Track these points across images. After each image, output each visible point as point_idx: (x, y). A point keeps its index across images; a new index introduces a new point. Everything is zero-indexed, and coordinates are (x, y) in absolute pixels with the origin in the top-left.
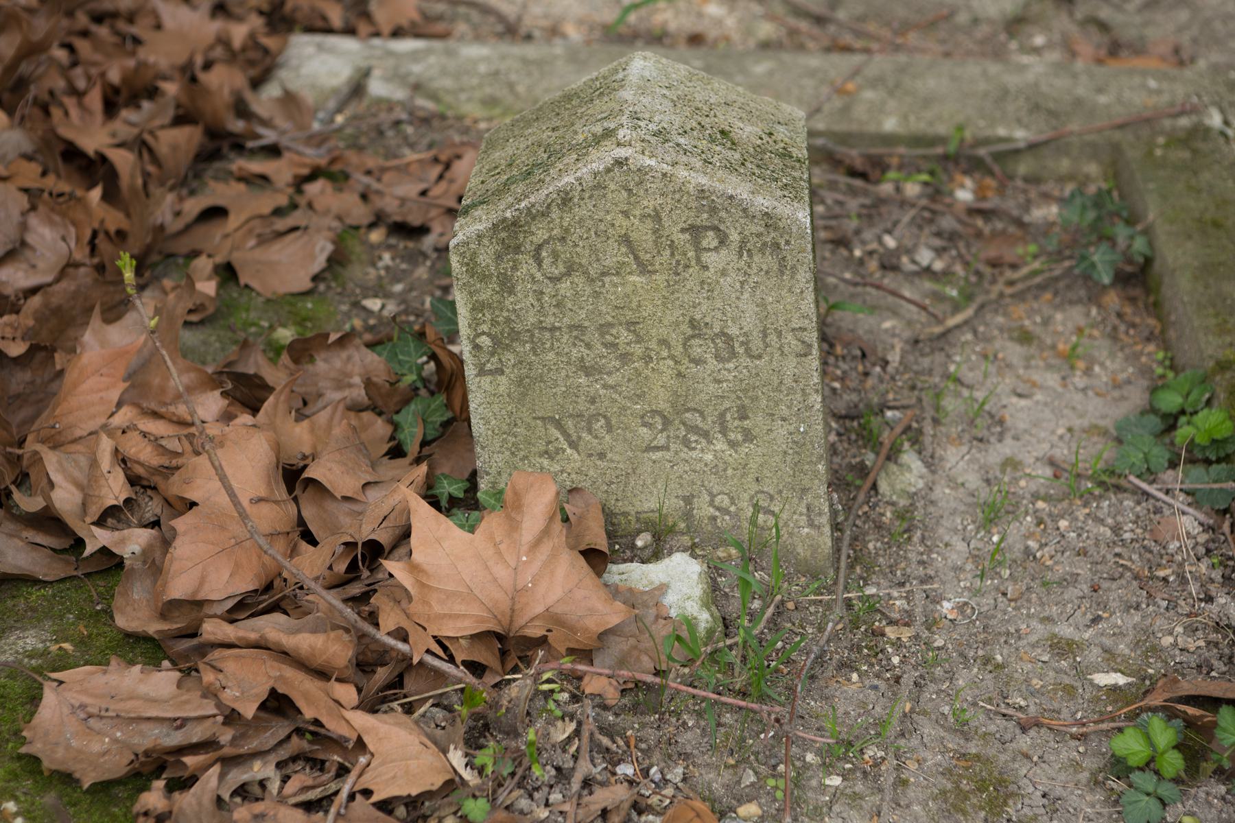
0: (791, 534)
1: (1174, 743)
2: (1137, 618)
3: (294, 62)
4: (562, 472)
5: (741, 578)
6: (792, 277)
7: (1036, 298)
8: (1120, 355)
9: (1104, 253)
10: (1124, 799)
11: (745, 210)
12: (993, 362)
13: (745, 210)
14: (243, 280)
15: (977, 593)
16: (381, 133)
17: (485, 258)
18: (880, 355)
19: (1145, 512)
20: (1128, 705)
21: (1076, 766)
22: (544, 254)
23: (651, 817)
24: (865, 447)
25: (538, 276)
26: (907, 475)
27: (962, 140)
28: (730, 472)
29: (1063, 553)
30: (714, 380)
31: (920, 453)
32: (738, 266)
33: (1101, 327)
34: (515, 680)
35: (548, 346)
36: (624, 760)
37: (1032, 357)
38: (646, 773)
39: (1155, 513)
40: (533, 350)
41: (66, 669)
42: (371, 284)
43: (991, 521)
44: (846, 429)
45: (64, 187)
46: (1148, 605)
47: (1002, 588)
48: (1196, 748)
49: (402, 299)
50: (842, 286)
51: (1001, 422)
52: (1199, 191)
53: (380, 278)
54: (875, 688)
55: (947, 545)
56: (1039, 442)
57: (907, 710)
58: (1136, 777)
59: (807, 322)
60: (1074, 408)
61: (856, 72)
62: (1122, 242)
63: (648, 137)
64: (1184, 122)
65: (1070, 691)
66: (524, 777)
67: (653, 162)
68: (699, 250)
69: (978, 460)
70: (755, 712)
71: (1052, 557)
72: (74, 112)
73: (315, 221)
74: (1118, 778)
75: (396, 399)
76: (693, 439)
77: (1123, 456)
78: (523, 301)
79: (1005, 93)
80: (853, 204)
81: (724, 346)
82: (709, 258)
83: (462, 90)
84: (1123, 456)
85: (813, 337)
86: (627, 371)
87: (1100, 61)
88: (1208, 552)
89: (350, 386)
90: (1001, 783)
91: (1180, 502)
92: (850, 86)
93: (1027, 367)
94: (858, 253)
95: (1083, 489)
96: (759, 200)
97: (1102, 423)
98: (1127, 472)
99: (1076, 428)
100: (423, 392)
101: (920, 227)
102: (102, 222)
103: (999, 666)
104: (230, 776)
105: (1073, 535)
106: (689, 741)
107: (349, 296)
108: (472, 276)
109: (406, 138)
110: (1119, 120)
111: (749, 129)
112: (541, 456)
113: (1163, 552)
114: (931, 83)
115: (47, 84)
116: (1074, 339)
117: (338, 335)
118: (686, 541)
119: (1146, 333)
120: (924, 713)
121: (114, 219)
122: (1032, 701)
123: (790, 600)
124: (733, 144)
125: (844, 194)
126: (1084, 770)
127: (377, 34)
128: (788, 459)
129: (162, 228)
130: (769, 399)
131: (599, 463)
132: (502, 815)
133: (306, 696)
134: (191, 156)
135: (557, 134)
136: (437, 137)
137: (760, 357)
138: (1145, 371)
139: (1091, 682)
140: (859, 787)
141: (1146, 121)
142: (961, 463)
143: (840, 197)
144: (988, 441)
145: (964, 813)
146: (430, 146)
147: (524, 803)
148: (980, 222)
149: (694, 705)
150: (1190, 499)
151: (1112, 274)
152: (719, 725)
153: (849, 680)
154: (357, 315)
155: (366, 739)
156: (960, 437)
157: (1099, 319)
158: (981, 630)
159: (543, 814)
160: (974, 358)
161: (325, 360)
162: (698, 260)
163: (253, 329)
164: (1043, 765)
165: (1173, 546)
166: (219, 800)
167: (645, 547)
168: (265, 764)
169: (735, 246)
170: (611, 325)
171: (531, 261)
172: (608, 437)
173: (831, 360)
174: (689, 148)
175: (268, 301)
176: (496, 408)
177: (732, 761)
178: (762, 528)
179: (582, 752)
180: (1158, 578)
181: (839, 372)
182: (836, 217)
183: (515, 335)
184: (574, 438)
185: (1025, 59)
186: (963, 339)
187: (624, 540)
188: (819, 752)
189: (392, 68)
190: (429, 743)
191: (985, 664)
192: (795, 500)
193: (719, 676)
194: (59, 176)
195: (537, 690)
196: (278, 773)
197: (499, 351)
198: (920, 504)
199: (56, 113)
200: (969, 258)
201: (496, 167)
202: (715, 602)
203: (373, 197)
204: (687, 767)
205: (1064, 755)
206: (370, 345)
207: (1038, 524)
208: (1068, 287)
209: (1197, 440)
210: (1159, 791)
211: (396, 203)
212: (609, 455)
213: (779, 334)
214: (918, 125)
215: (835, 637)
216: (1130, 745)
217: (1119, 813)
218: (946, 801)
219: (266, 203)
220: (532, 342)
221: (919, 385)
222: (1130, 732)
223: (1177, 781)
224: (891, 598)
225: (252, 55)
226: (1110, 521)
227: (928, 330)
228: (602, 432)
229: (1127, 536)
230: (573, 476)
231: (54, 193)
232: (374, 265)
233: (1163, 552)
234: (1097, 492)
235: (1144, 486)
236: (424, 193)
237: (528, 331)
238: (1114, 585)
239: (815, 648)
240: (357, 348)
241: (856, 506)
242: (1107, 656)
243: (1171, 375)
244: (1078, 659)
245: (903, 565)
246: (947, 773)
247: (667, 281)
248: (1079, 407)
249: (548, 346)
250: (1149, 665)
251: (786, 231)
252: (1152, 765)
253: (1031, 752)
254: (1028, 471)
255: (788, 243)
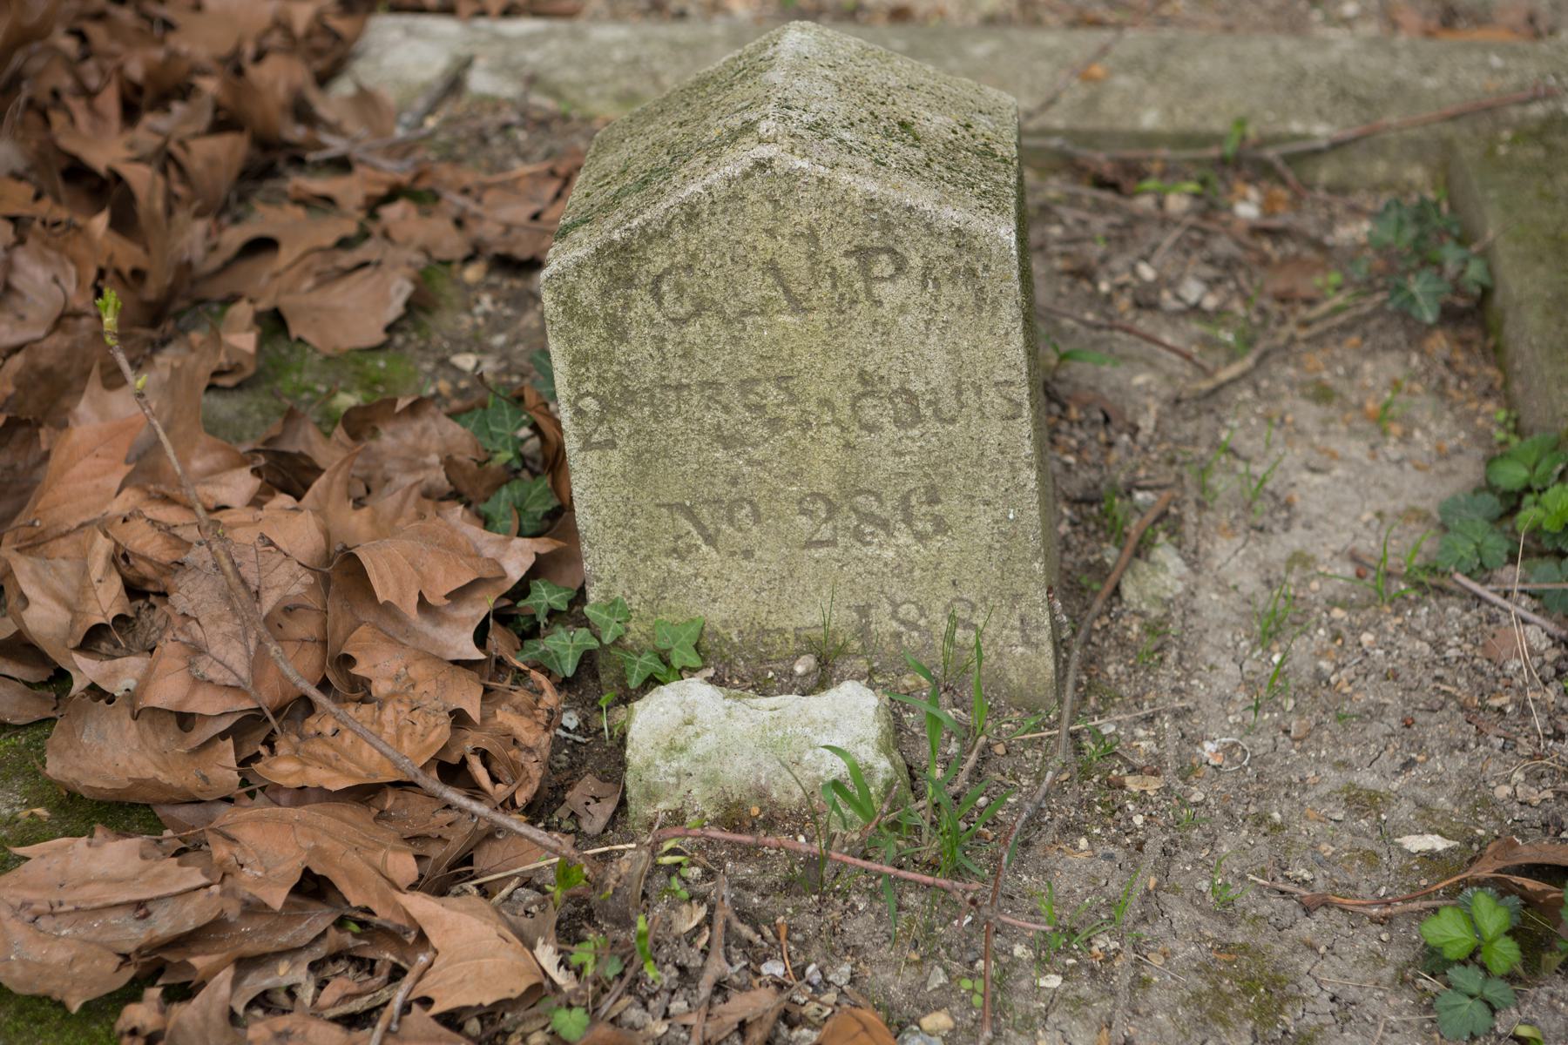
0: (1000, 655)
1: (1507, 928)
2: (1463, 762)
3: (374, 51)
4: (696, 576)
5: (928, 713)
6: (993, 315)
7: (1339, 342)
8: (1448, 415)
9: (1426, 283)
10: (1439, 1003)
11: (928, 226)
12: (1278, 427)
13: (928, 226)
14: (295, 331)
15: (1250, 730)
16: (484, 140)
17: (588, 294)
18: (1129, 419)
19: (1476, 621)
20: (1448, 876)
21: (1377, 959)
22: (665, 288)
23: (805, 1032)
24: (1107, 540)
25: (658, 317)
26: (1162, 576)
27: (1243, 138)
28: (917, 573)
29: (1366, 676)
30: (894, 451)
31: (1179, 546)
32: (923, 300)
33: (1425, 379)
34: (622, 853)
35: (673, 409)
36: (771, 957)
37: (1332, 420)
38: (800, 973)
39: (1489, 623)
40: (654, 414)
41: (37, 841)
42: (464, 336)
43: (1270, 635)
44: (1082, 517)
45: (62, 214)
46: (1478, 745)
47: (1284, 724)
48: (1533, 938)
49: (504, 354)
50: (1082, 330)
51: (1288, 505)
52: (1554, 200)
53: (476, 327)
54: (1110, 857)
55: (1212, 667)
56: (1337, 531)
57: (1151, 886)
58: (1456, 974)
59: (1015, 373)
60: (1385, 486)
61: (1104, 51)
62: (1451, 267)
63: (800, 132)
64: (1537, 110)
65: (1371, 859)
66: (636, 980)
67: (805, 164)
68: (869, 279)
69: (1256, 555)
70: (947, 892)
71: (1350, 682)
72: (82, 118)
73: (392, 253)
74: (1433, 975)
75: (487, 483)
76: (867, 530)
77: (1447, 548)
78: (639, 349)
79: (1302, 75)
80: (1099, 224)
81: (905, 406)
82: (883, 290)
83: (591, 83)
84: (1447, 548)
85: (1022, 393)
86: (779, 441)
87: (1429, 34)
88: (1559, 673)
89: (426, 467)
90: (1275, 982)
91: (1524, 606)
92: (1097, 70)
93: (1324, 433)
94: (1104, 287)
95: (1393, 592)
96: (948, 212)
97: (1422, 505)
98: (1452, 569)
99: (1388, 512)
100: (525, 474)
101: (1187, 253)
102: (111, 258)
103: (1277, 828)
104: (246, 982)
105: (1380, 652)
106: (859, 930)
107: (434, 351)
108: (571, 319)
109: (516, 146)
110: (1451, 110)
111: (939, 119)
112: (668, 555)
113: (1498, 673)
114: (1203, 65)
115: (49, 82)
116: (1388, 395)
117: (409, 401)
118: (861, 664)
119: (1483, 387)
120: (1175, 890)
121: (127, 255)
122: (1319, 873)
123: (1000, 741)
124: (916, 139)
125: (1089, 211)
126: (1387, 964)
127: (483, 13)
128: (994, 555)
129: (189, 265)
130: (967, 476)
131: (744, 563)
132: (604, 1030)
133: (351, 875)
134: (234, 172)
135: (685, 130)
136: (558, 144)
137: (953, 421)
138: (1481, 437)
139: (1400, 847)
140: (1085, 989)
141: (1486, 110)
142: (1234, 560)
143: (1082, 215)
144: (1271, 531)
145: (1225, 1023)
146: (549, 155)
147: (635, 1015)
148: (1267, 245)
149: (867, 882)
150: (1536, 604)
151: (1437, 309)
152: (900, 908)
153: (1075, 847)
154: (445, 377)
155: (427, 930)
156: (1232, 526)
157: (1422, 369)
158: (1254, 779)
159: (660, 1028)
160: (1254, 421)
161: (394, 435)
162: (869, 293)
163: (306, 396)
164: (1333, 958)
165: (1511, 666)
166: (232, 1017)
167: (807, 674)
168: (294, 965)
169: (917, 273)
170: (756, 381)
171: (648, 298)
172: (755, 530)
173: (1064, 426)
174: (855, 145)
175: (328, 359)
176: (607, 492)
177: (915, 957)
178: (962, 648)
179: (714, 946)
180: (1491, 708)
181: (1073, 443)
182: (1075, 241)
183: (629, 396)
184: (711, 531)
185: (1332, 33)
186: (1240, 397)
187: (780, 666)
188: (1030, 945)
189: (501, 57)
190: (510, 935)
191: (1257, 825)
192: (1005, 610)
193: (900, 843)
194: (57, 200)
195: (657, 866)
196: (312, 977)
197: (609, 417)
198: (1176, 615)
199: (58, 119)
200: (1250, 291)
201: (606, 176)
202: (898, 744)
203: (470, 223)
204: (856, 965)
205: (1361, 944)
206: (453, 415)
207: (1334, 639)
208: (1381, 328)
209: (1546, 526)
210: (1487, 992)
211: (498, 229)
212: (758, 554)
213: (979, 391)
214: (1185, 120)
215: (1059, 789)
216: (1448, 931)
217: (1433, 1021)
218: (1200, 1008)
219: (330, 231)
220: (653, 404)
221: (1180, 458)
222: (1446, 913)
223: (1511, 978)
224: (1135, 738)
225: (320, 41)
226: (1429, 634)
227: (1193, 386)
228: (748, 523)
229: (1452, 653)
230: (712, 581)
231: (49, 221)
232: (469, 310)
233: (1498, 673)
234: (1412, 595)
235: (1475, 587)
236: (536, 217)
237: (647, 390)
238: (1433, 719)
239: (1028, 806)
240: (435, 417)
241: (1089, 618)
242: (1423, 812)
243: (1515, 441)
244: (1384, 817)
245: (1152, 694)
246: (1204, 969)
247: (828, 321)
248: (1392, 484)
249: (673, 409)
250: (1478, 824)
251: (981, 253)
252: (1479, 958)
253: (1317, 941)
254: (1322, 569)
255: (986, 268)
